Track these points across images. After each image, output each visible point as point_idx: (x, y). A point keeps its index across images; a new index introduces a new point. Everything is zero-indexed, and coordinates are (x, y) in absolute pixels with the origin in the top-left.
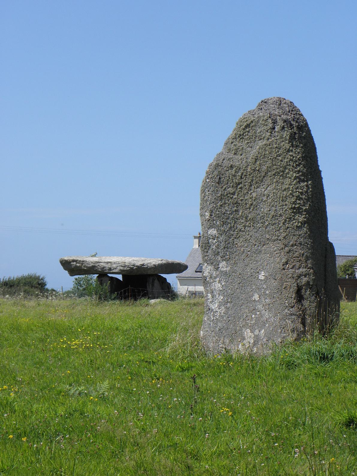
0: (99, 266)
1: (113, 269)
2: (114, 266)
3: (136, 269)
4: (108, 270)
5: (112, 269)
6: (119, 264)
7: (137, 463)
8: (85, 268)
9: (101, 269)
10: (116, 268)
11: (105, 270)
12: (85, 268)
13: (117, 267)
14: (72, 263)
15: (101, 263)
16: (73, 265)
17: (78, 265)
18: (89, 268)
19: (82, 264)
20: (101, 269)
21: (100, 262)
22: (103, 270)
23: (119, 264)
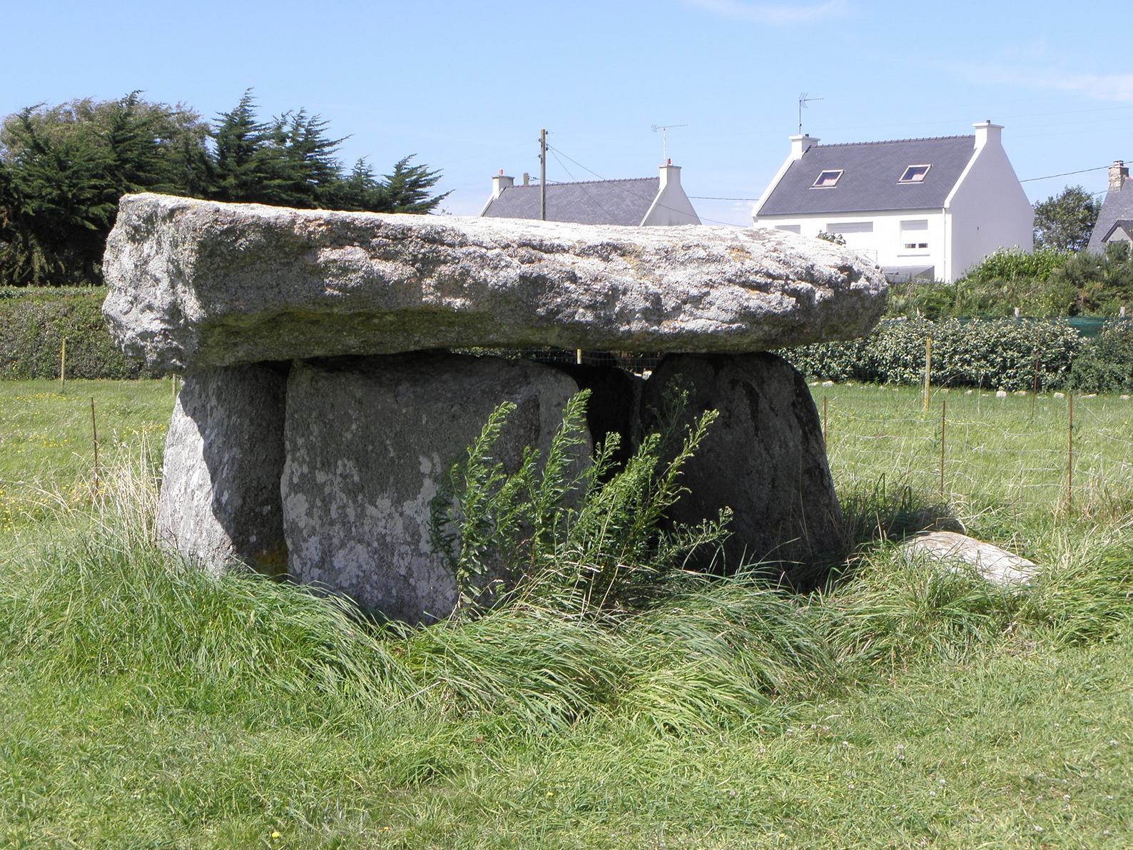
0: (573, 278)
1: (677, 310)
2: (682, 279)
3: (826, 302)
4: (646, 314)
5: (669, 303)
6: (711, 259)
7: (128, 115)
8: (458, 302)
9: (591, 307)
10: (697, 301)
11: (626, 316)
12: (458, 302)
13: (711, 285)
14: (327, 254)
15: (559, 257)
16: (345, 269)
17: (386, 268)
18: (502, 296)
19: (426, 264)
20: (591, 307)
21: (551, 250)
22: (609, 321)
23: (711, 259)
